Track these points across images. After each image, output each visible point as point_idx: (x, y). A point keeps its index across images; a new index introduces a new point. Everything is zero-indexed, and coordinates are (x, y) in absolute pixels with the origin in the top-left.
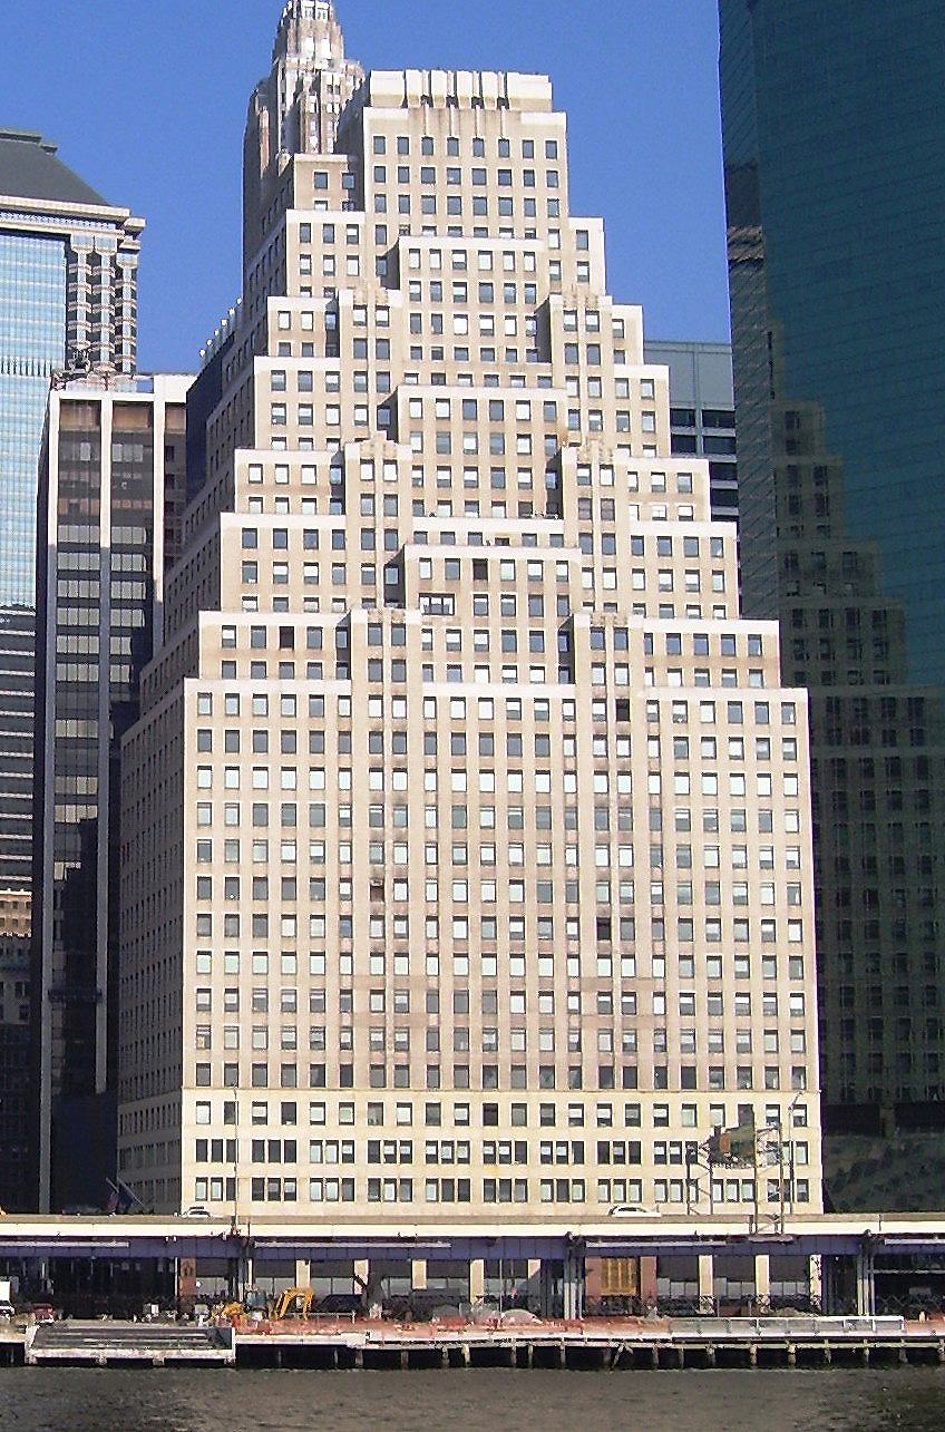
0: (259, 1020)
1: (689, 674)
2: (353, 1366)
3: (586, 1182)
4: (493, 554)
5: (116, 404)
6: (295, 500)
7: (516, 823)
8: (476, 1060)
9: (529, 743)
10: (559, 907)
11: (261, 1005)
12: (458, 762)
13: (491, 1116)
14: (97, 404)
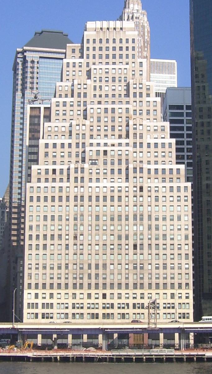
0: (44, 272)
1: (160, 179)
2: (29, 361)
3: (129, 314)
4: (108, 149)
5: (45, 108)
6: (60, 135)
7: (112, 219)
8: (101, 281)
9: (116, 198)
10: (123, 241)
11: (45, 268)
12: (97, 203)
13: (104, 296)
14: (40, 108)
